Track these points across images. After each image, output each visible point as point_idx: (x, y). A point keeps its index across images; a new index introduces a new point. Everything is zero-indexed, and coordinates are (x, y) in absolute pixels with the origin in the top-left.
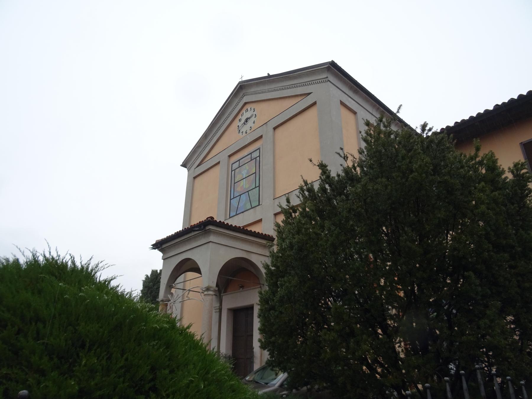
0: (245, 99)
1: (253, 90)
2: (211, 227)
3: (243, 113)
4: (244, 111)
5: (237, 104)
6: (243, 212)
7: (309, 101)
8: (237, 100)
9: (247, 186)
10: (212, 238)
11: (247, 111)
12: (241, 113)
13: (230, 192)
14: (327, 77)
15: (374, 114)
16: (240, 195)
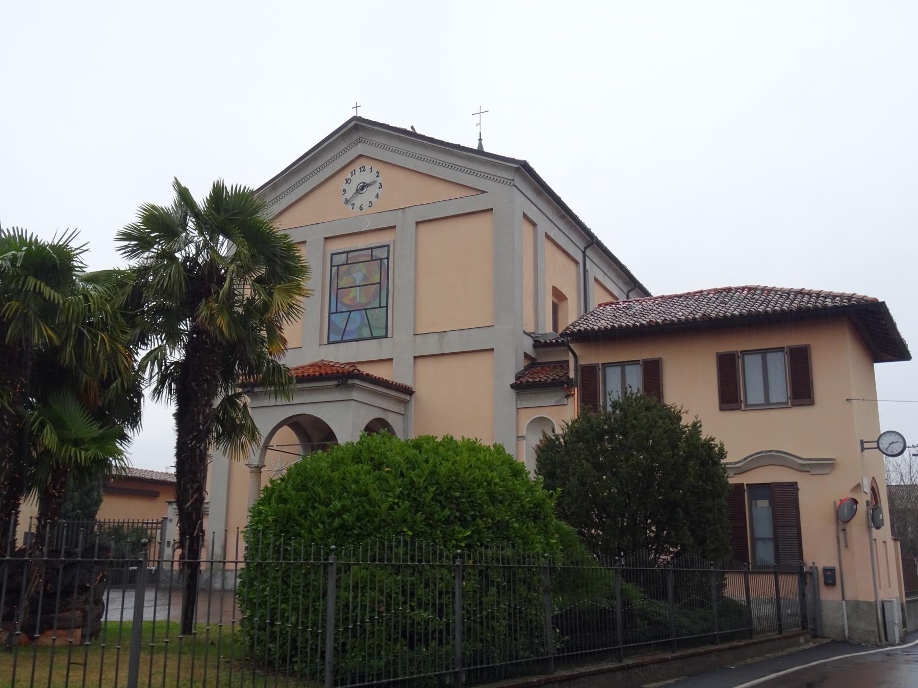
0: (360, 149)
1: (379, 140)
2: (357, 382)
3: (355, 171)
4: (357, 166)
5: (345, 151)
6: (357, 340)
7: (480, 203)
8: (344, 145)
9: (364, 301)
10: (355, 395)
11: (362, 169)
12: (351, 169)
13: (328, 300)
14: (513, 180)
15: (553, 221)
16: (350, 312)
